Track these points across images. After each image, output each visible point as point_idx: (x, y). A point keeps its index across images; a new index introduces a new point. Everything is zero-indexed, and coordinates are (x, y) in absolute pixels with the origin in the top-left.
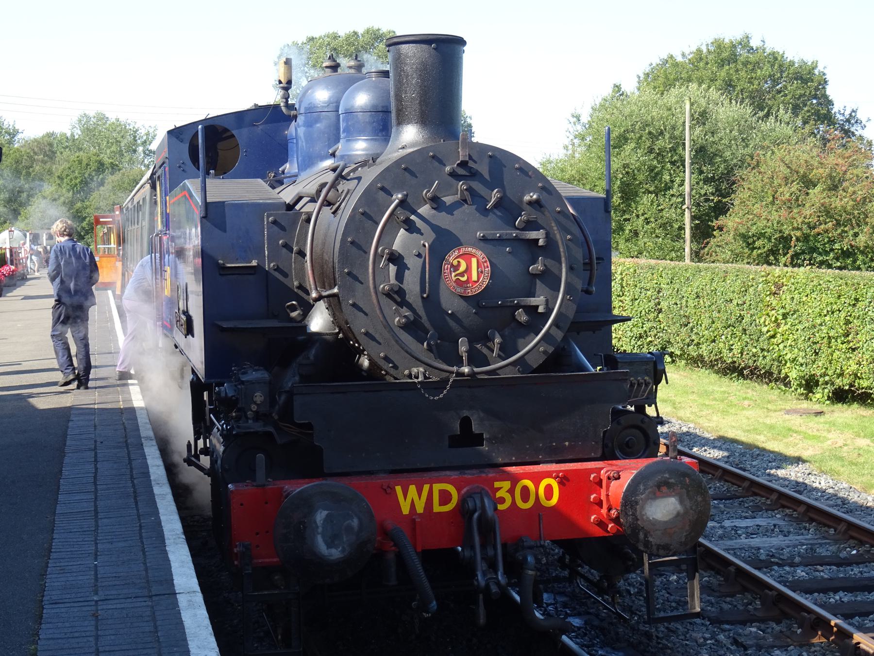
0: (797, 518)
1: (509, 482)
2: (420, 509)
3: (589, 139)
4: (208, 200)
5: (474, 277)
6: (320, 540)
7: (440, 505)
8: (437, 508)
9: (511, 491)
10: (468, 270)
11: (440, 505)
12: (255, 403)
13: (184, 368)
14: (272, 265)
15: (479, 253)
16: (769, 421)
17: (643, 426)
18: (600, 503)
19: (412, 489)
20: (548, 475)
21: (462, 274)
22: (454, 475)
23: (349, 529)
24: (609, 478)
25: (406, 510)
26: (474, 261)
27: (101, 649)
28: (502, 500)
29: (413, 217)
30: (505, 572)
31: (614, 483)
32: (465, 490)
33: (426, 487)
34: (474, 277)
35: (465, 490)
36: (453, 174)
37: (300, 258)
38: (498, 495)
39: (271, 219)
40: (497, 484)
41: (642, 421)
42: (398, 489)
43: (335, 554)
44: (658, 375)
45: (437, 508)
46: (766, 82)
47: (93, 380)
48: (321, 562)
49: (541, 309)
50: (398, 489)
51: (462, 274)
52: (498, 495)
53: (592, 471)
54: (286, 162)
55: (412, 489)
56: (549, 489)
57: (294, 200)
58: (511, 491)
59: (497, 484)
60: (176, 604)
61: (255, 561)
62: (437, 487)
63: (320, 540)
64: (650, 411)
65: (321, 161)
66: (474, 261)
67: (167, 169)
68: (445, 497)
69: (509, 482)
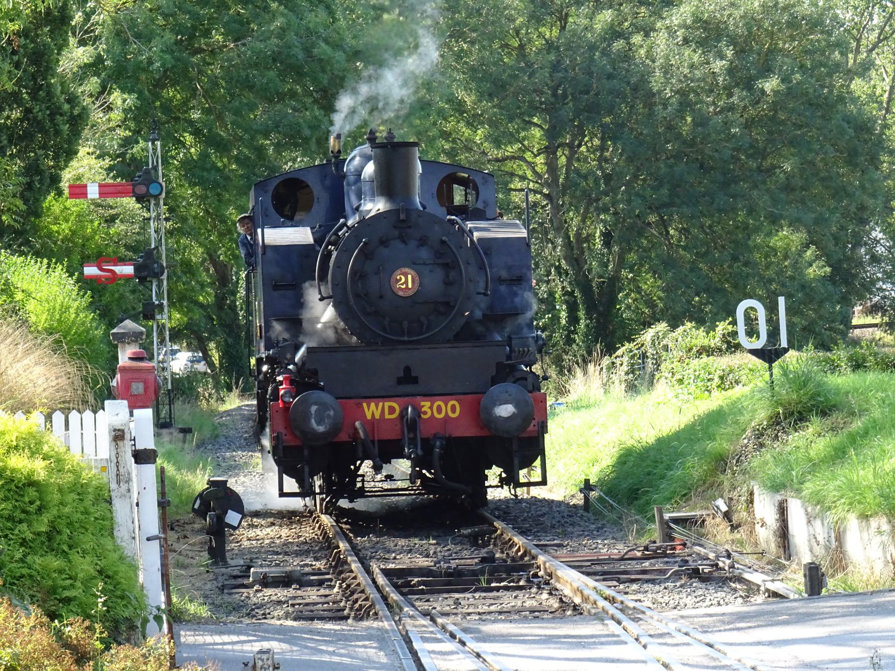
0: (546, 109)
2: (377, 416)
5: (410, 286)
6: (313, 421)
7: (390, 414)
8: (387, 416)
10: (406, 282)
11: (390, 414)
15: (413, 272)
16: (563, 313)
19: (373, 405)
21: (402, 284)
23: (329, 416)
25: (369, 417)
26: (410, 277)
28: (425, 413)
30: (422, 449)
33: (381, 404)
34: (410, 286)
38: (423, 409)
42: (365, 405)
43: (321, 429)
45: (387, 416)
48: (315, 434)
51: (402, 284)
52: (423, 409)
55: (373, 405)
57: (533, 646)
58: (431, 408)
59: (422, 403)
62: (387, 404)
63: (313, 421)
66: (410, 277)
68: (392, 410)
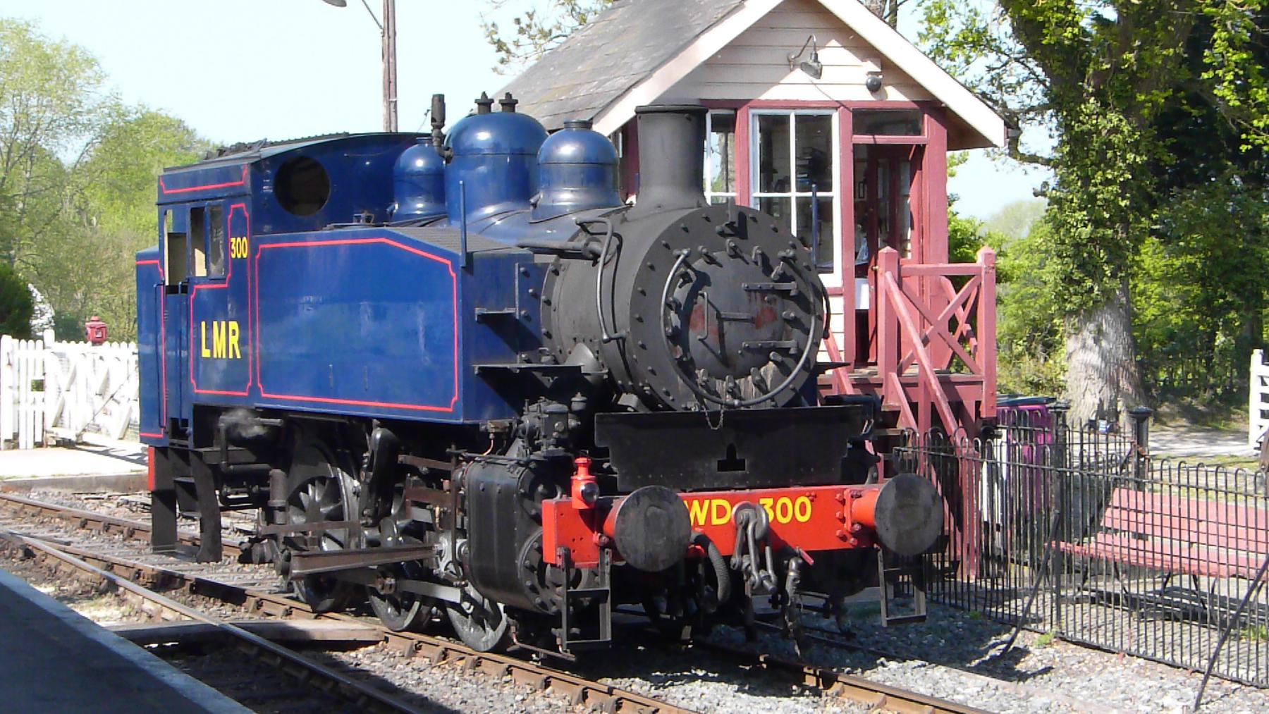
3: (973, 238)
8: (715, 521)
9: (773, 508)
14: (523, 312)
18: (843, 520)
20: (802, 494)
24: (852, 497)
29: (689, 270)
31: (856, 502)
33: (707, 503)
36: (722, 234)
37: (546, 306)
39: (522, 269)
45: (715, 521)
46: (1086, 226)
49: (792, 351)
53: (837, 491)
54: (393, 201)
56: (803, 506)
58: (773, 508)
62: (715, 502)
65: (410, 196)
68: (721, 512)
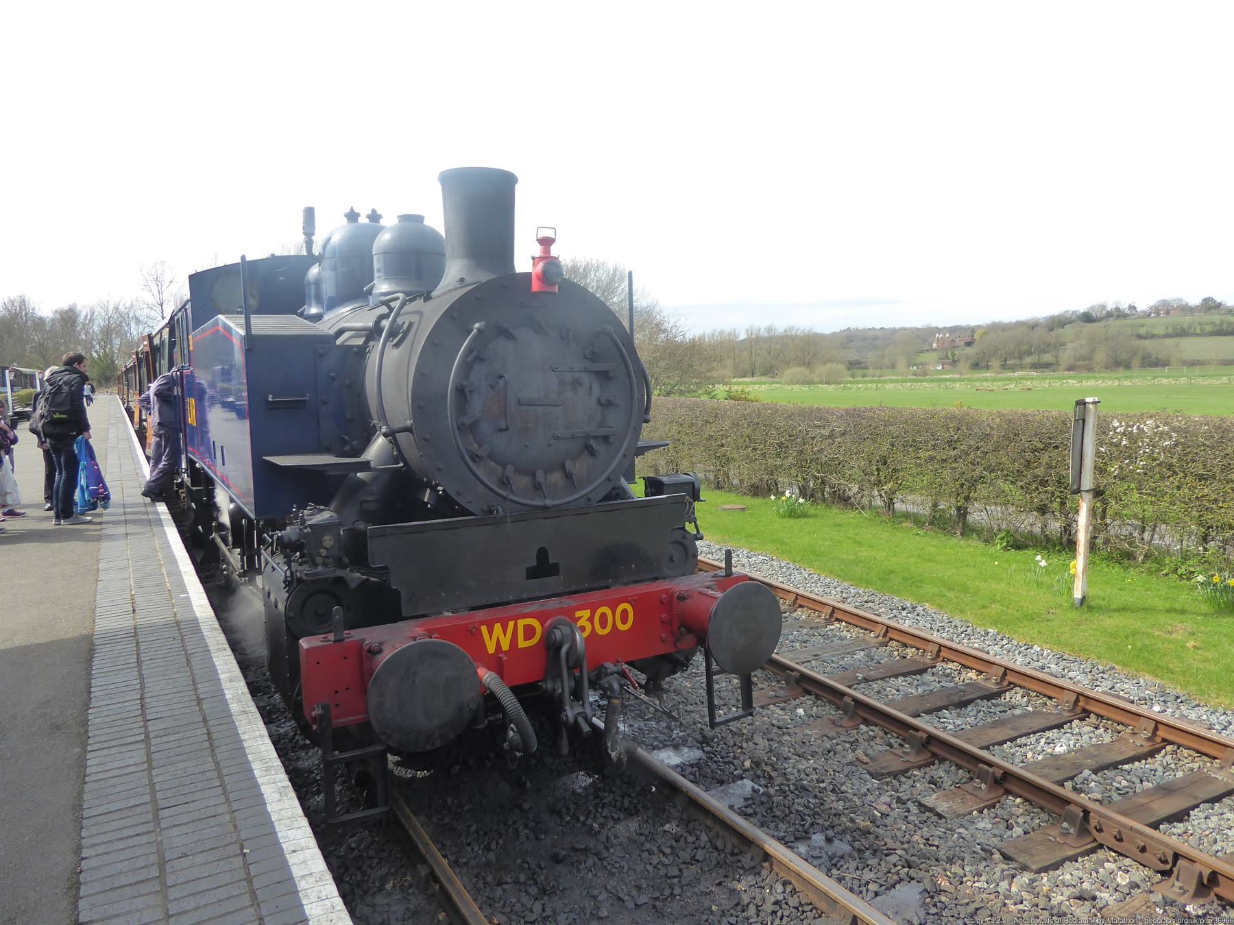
1: (589, 611)
4: (254, 332)
8: (522, 644)
9: (591, 620)
12: (324, 548)
13: (747, 868)
17: (683, 541)
19: (498, 627)
20: (624, 600)
22: (534, 607)
25: (491, 649)
27: (162, 804)
32: (549, 622)
33: (511, 624)
35: (549, 622)
38: (580, 623)
40: (578, 614)
41: (684, 537)
42: (484, 629)
44: (696, 496)
45: (522, 644)
47: (246, 893)
50: (484, 629)
55: (498, 627)
58: (591, 620)
60: (294, 881)
61: (336, 721)
62: (522, 623)
64: (689, 527)
67: (189, 311)
68: (529, 632)
69: (589, 611)
